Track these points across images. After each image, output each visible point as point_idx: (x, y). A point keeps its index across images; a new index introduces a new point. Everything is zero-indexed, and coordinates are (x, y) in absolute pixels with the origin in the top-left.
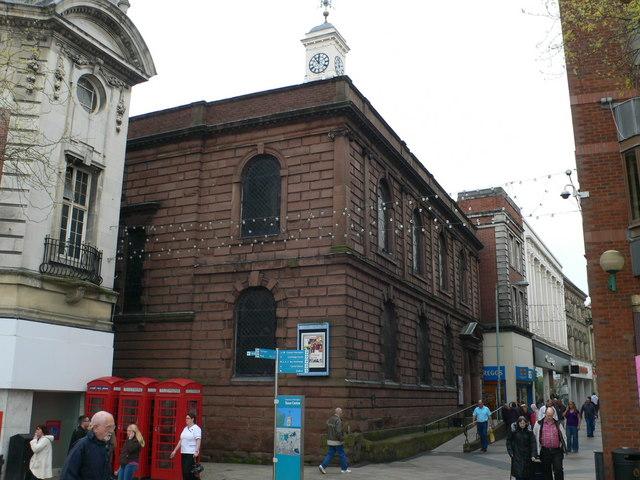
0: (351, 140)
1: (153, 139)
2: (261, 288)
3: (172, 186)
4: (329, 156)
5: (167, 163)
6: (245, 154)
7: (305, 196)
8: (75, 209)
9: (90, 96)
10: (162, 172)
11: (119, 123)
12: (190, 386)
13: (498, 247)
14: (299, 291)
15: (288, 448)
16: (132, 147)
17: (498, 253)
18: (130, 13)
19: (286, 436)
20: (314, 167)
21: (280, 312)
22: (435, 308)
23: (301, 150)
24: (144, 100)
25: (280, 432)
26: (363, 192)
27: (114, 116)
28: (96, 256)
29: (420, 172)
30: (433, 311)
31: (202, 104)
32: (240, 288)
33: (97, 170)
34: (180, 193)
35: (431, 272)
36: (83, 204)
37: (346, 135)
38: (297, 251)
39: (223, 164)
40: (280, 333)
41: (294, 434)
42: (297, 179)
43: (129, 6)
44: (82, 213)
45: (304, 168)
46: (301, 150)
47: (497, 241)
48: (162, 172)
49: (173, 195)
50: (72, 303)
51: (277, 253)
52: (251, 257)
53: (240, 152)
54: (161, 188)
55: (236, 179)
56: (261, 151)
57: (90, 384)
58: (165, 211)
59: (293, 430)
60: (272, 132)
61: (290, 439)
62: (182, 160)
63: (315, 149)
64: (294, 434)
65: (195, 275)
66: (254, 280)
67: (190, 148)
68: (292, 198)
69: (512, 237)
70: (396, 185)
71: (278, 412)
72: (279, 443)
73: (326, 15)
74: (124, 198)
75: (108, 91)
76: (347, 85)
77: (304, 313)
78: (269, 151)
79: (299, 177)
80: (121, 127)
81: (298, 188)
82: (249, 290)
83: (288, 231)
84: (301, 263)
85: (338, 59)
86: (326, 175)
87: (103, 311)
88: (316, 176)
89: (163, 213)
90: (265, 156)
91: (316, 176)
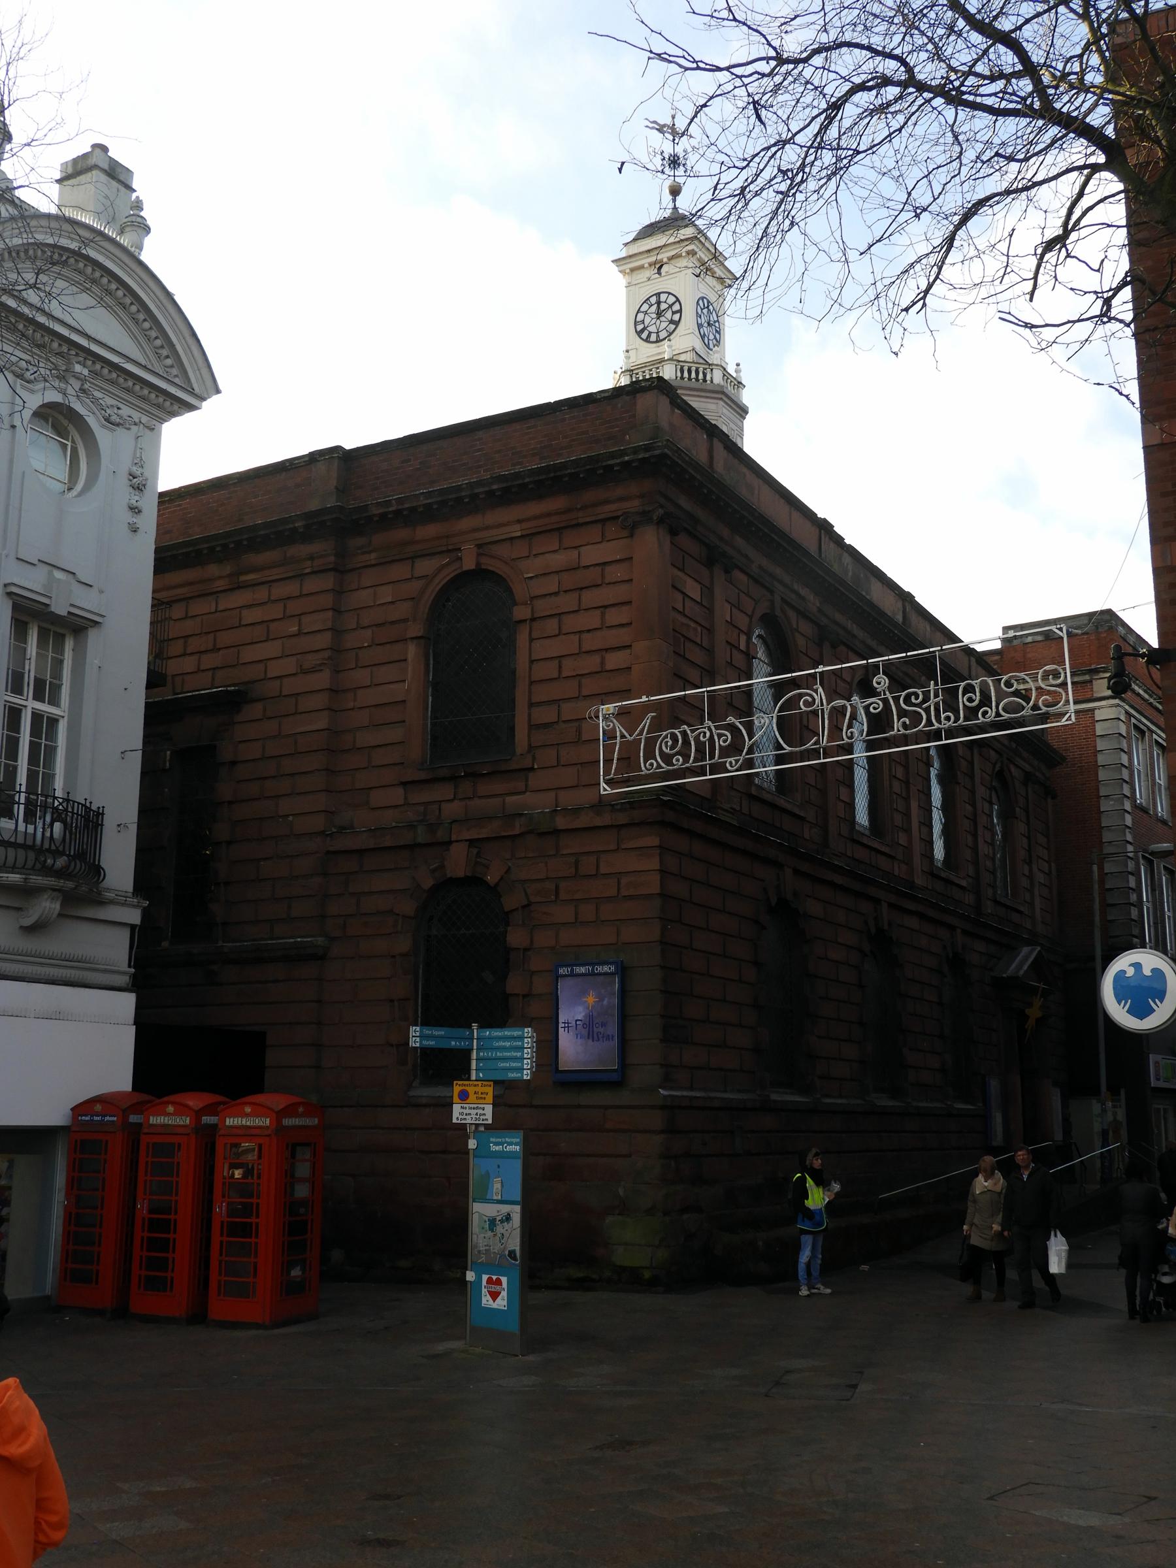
0: (673, 532)
1: (220, 541)
2: (474, 881)
3: (271, 649)
4: (617, 573)
5: (261, 594)
6: (433, 571)
7: (569, 668)
8: (37, 717)
9: (64, 446)
10: (250, 616)
11: (135, 510)
12: (289, 1111)
13: (1101, 759)
14: (557, 888)
15: (497, 1248)
16: (167, 560)
17: (1102, 775)
18: (152, 254)
19: (492, 1222)
20: (589, 598)
21: (516, 938)
22: (922, 916)
23: (559, 559)
24: (193, 451)
25: (480, 1211)
26: (710, 651)
27: (125, 496)
28: (89, 822)
29: (876, 593)
30: (913, 922)
31: (338, 449)
32: (428, 883)
33: (75, 627)
34: (290, 665)
35: (908, 831)
36: (54, 702)
37: (660, 522)
38: (552, 794)
39: (386, 594)
40: (514, 984)
41: (508, 1218)
42: (552, 626)
43: (147, 230)
44: (53, 722)
45: (567, 602)
46: (559, 559)
47: (1101, 745)
48: (250, 616)
49: (275, 670)
50: (35, 929)
51: (509, 799)
52: (453, 809)
53: (425, 566)
54: (250, 654)
55: (416, 629)
56: (469, 564)
57: (78, 1110)
58: (259, 706)
59: (505, 1209)
60: (491, 517)
61: (499, 1229)
62: (291, 588)
63: (593, 554)
64: (508, 1218)
65: (328, 852)
66: (458, 862)
67: (312, 558)
68: (540, 671)
69: (1142, 733)
70: (806, 628)
71: (477, 1167)
72: (479, 1237)
73: (675, 191)
74: (154, 680)
75: (103, 436)
76: (664, 402)
77: (917, 847)
78: (489, 564)
79: (555, 621)
80: (138, 520)
81: (553, 648)
82: (447, 884)
83: (531, 748)
84: (561, 823)
85: (704, 305)
86: (614, 617)
87: (113, 948)
88: (593, 620)
89: (255, 710)
90: (480, 573)
91: (593, 620)
